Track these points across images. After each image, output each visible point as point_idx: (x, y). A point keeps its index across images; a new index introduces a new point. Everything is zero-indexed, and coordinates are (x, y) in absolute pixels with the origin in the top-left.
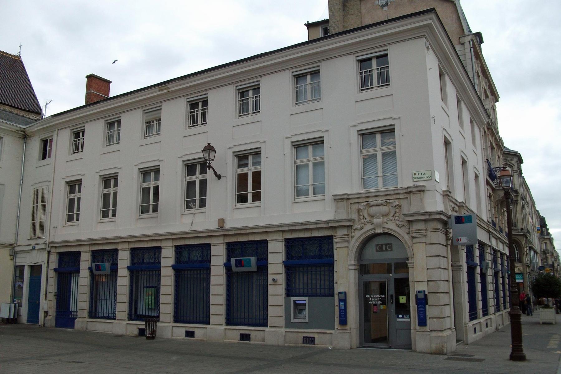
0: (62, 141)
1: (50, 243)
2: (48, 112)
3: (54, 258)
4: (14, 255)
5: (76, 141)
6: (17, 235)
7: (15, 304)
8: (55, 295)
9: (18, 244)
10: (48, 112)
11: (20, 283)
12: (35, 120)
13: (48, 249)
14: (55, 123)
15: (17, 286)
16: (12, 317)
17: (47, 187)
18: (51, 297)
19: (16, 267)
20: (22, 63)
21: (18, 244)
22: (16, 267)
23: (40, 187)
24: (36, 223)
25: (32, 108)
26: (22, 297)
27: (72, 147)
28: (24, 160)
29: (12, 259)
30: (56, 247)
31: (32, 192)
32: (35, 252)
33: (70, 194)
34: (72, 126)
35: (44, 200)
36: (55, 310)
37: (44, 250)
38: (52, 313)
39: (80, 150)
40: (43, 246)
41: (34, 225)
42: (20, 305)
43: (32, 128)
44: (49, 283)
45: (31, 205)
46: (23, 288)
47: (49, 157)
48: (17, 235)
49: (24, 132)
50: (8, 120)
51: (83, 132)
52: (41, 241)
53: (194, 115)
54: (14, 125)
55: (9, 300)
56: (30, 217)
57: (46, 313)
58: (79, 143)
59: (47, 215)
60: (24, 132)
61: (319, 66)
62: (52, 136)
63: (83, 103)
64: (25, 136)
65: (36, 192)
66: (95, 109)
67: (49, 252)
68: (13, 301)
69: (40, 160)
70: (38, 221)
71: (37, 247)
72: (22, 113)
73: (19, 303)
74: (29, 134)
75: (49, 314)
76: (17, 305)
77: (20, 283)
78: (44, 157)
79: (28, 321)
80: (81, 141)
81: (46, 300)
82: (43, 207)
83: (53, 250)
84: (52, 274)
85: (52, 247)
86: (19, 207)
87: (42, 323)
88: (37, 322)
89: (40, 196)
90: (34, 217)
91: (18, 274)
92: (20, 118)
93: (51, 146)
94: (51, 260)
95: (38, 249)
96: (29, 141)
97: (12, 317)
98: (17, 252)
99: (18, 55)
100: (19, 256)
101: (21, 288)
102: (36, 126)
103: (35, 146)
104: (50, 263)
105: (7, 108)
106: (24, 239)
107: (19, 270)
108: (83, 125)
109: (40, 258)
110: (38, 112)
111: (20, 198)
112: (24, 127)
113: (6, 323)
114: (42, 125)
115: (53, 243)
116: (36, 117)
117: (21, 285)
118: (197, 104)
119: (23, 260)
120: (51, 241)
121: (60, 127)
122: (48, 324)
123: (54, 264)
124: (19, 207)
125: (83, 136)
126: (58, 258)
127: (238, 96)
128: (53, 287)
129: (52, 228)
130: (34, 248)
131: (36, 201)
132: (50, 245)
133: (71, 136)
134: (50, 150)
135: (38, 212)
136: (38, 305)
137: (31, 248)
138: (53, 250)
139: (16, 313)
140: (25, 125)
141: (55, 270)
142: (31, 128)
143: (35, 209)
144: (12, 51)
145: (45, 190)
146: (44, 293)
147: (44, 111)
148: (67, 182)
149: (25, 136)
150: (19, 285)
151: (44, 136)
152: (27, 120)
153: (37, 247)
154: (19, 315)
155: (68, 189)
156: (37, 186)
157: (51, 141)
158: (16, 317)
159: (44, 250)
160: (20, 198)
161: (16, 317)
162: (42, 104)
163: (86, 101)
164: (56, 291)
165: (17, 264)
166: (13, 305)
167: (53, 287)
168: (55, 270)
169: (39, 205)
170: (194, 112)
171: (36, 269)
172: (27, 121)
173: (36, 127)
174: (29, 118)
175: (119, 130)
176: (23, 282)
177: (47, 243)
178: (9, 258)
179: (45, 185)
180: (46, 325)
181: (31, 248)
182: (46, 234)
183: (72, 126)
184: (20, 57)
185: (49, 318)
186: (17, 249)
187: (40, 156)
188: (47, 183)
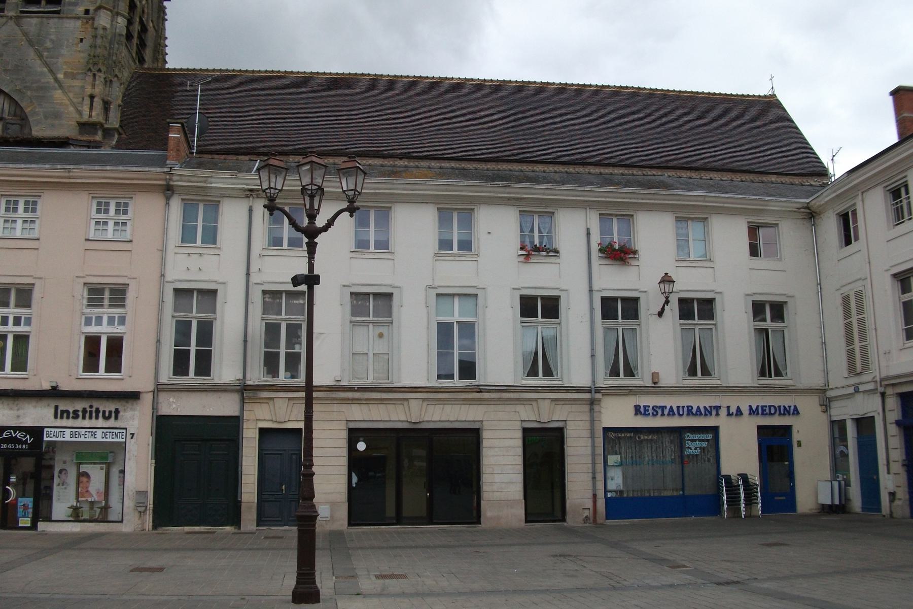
0: (873, 210)
1: (882, 380)
2: (838, 169)
3: (893, 403)
4: (826, 405)
5: (897, 203)
6: (826, 372)
7: (839, 482)
8: (903, 465)
9: (831, 386)
10: (838, 169)
11: (843, 448)
12: (821, 186)
13: (881, 389)
14: (855, 182)
15: (838, 452)
16: (837, 502)
17: (862, 288)
18: (897, 467)
19: (833, 423)
20: (779, 104)
21: (831, 386)
22: (833, 423)
23: (850, 290)
24: (853, 349)
25: (812, 169)
26: (848, 470)
27: (892, 216)
28: (816, 251)
29: (825, 411)
30: (893, 385)
31: (839, 301)
32: (859, 397)
33: (903, 294)
34: (884, 181)
35: (860, 309)
36: (906, 489)
37: (874, 391)
38: (903, 494)
39: (906, 217)
40: (871, 386)
41: (851, 354)
42: (848, 484)
43: (819, 199)
44: (890, 446)
45: (841, 322)
46: (847, 455)
47: (857, 239)
48: (826, 372)
49: (808, 208)
50: (781, 195)
51: (906, 187)
52: (866, 378)
53: (897, 208)
54: (791, 202)
55: (828, 476)
56: (842, 342)
57: (892, 495)
58: (902, 207)
59: (871, 334)
60: (808, 208)
61: (905, 177)
62: (854, 204)
63: (894, 139)
64: (811, 215)
65: (846, 300)
66: (887, 161)
67: (883, 395)
68: (834, 478)
69: (842, 247)
70: (857, 346)
71: (862, 388)
72: (797, 180)
73: (844, 480)
74: (817, 211)
75: (898, 496)
76: (843, 483)
77: (843, 448)
78: (848, 242)
79: (863, 509)
80: (905, 203)
81: (889, 473)
82: (861, 322)
83: (889, 391)
84: (893, 430)
85: (887, 385)
86: (822, 328)
87: (888, 512)
88: (879, 510)
89: (853, 305)
90: (849, 340)
91: (837, 435)
92: (796, 188)
93: (855, 220)
94: (888, 407)
95: (864, 392)
96: (818, 221)
97: (837, 502)
98: (830, 400)
99: (771, 93)
100: (834, 404)
101: (845, 455)
102: (825, 194)
103: (830, 227)
104: (887, 413)
105: (773, 178)
106: (839, 377)
107: (838, 427)
108: (903, 175)
109: (869, 406)
110: (823, 173)
111: (821, 314)
112: (807, 201)
113: (829, 513)
114: (834, 192)
115: (887, 378)
116: (820, 181)
117: (845, 451)
118: (899, 190)
119: (839, 411)
120: (883, 375)
121: (864, 188)
122: (898, 513)
123: (894, 414)
124: (822, 328)
125: (907, 192)
126: (899, 403)
127: (890, 197)
128: (899, 450)
129: (881, 353)
130: (857, 391)
131: (847, 313)
132: (884, 383)
133: (885, 196)
134: (856, 229)
135: (855, 331)
136: (876, 483)
137: (851, 390)
138: (889, 391)
139: (843, 495)
140: (807, 197)
141: (898, 423)
142: (817, 201)
143: (848, 327)
144: (760, 89)
145: (859, 295)
146: (885, 462)
147: (831, 171)
148: (895, 276)
149: (811, 215)
150: (842, 452)
151: (841, 208)
152: (809, 188)
153: (862, 388)
154: (848, 500)
155: (898, 286)
156: (845, 290)
157: (854, 213)
158: (843, 502)
159: (874, 391)
160: (821, 314)
161: (843, 502)
162: (825, 159)
163: (900, 134)
164: (904, 458)
165: (834, 419)
166: (836, 484)
167: (899, 450)
168: (898, 423)
169: (854, 320)
170: (897, 203)
171: (865, 424)
172: (810, 191)
173: (826, 196)
174: (811, 185)
175: (909, 198)
176: (846, 446)
177: (878, 380)
178: (819, 409)
179: (858, 286)
180: (895, 515)
181: (851, 390)
182: (874, 366)
183: (884, 181)
184: (774, 96)
185: (897, 502)
186: (830, 394)
187: (840, 241)
188: (860, 283)
